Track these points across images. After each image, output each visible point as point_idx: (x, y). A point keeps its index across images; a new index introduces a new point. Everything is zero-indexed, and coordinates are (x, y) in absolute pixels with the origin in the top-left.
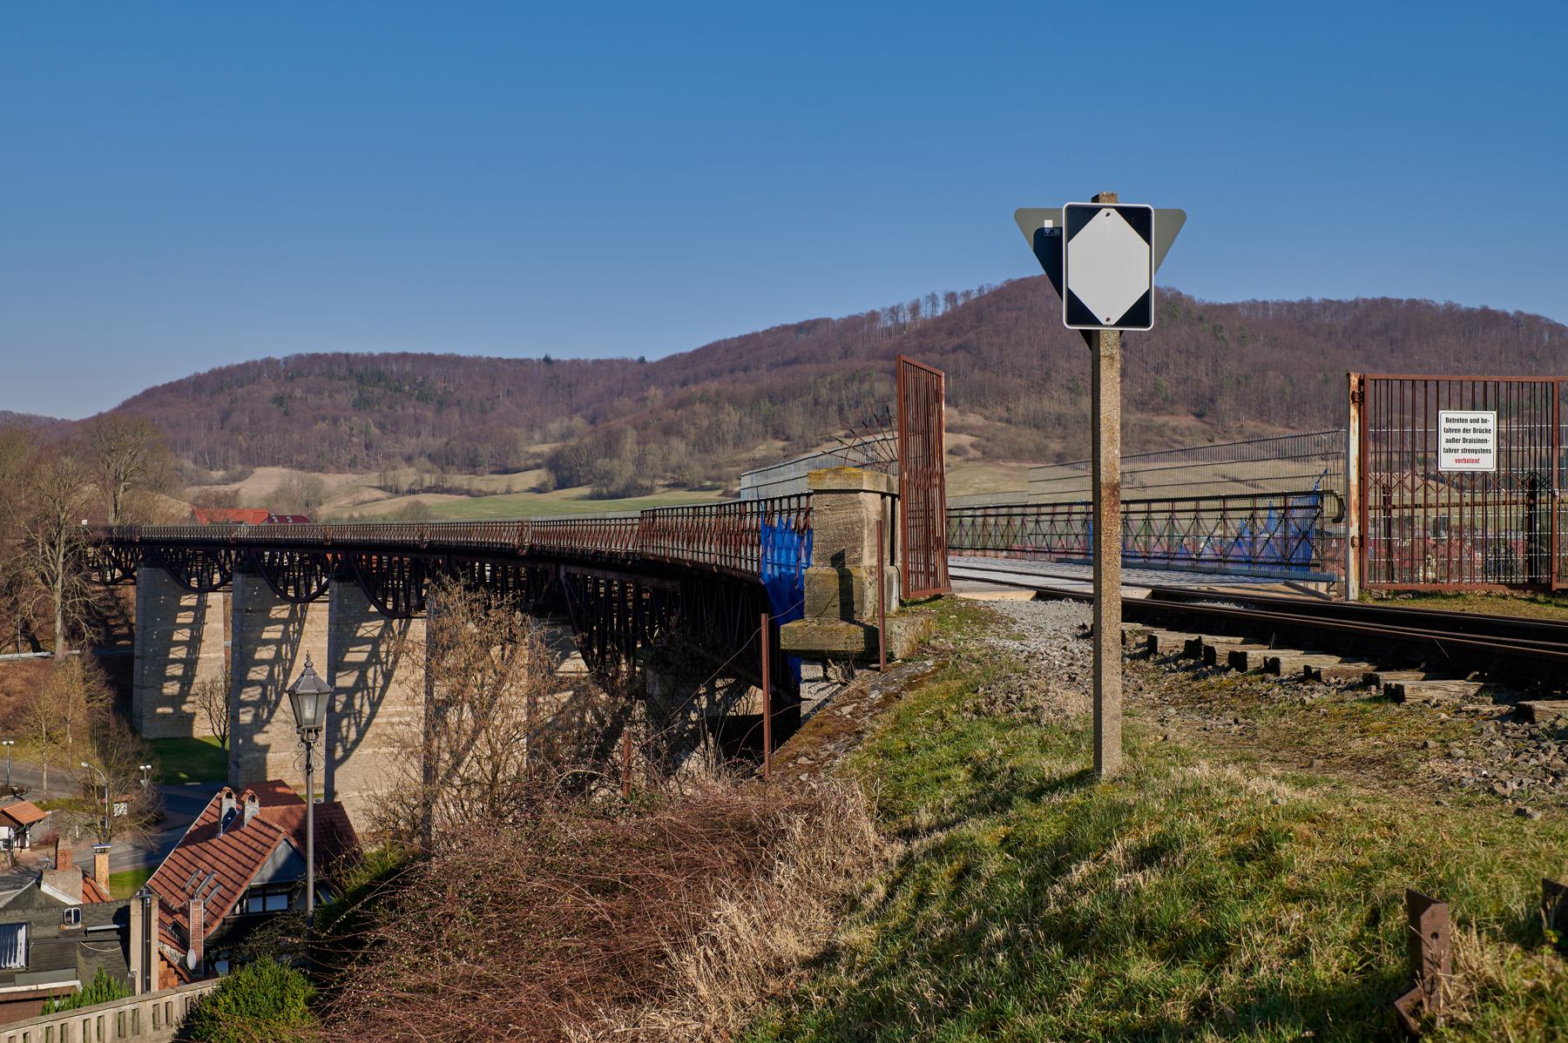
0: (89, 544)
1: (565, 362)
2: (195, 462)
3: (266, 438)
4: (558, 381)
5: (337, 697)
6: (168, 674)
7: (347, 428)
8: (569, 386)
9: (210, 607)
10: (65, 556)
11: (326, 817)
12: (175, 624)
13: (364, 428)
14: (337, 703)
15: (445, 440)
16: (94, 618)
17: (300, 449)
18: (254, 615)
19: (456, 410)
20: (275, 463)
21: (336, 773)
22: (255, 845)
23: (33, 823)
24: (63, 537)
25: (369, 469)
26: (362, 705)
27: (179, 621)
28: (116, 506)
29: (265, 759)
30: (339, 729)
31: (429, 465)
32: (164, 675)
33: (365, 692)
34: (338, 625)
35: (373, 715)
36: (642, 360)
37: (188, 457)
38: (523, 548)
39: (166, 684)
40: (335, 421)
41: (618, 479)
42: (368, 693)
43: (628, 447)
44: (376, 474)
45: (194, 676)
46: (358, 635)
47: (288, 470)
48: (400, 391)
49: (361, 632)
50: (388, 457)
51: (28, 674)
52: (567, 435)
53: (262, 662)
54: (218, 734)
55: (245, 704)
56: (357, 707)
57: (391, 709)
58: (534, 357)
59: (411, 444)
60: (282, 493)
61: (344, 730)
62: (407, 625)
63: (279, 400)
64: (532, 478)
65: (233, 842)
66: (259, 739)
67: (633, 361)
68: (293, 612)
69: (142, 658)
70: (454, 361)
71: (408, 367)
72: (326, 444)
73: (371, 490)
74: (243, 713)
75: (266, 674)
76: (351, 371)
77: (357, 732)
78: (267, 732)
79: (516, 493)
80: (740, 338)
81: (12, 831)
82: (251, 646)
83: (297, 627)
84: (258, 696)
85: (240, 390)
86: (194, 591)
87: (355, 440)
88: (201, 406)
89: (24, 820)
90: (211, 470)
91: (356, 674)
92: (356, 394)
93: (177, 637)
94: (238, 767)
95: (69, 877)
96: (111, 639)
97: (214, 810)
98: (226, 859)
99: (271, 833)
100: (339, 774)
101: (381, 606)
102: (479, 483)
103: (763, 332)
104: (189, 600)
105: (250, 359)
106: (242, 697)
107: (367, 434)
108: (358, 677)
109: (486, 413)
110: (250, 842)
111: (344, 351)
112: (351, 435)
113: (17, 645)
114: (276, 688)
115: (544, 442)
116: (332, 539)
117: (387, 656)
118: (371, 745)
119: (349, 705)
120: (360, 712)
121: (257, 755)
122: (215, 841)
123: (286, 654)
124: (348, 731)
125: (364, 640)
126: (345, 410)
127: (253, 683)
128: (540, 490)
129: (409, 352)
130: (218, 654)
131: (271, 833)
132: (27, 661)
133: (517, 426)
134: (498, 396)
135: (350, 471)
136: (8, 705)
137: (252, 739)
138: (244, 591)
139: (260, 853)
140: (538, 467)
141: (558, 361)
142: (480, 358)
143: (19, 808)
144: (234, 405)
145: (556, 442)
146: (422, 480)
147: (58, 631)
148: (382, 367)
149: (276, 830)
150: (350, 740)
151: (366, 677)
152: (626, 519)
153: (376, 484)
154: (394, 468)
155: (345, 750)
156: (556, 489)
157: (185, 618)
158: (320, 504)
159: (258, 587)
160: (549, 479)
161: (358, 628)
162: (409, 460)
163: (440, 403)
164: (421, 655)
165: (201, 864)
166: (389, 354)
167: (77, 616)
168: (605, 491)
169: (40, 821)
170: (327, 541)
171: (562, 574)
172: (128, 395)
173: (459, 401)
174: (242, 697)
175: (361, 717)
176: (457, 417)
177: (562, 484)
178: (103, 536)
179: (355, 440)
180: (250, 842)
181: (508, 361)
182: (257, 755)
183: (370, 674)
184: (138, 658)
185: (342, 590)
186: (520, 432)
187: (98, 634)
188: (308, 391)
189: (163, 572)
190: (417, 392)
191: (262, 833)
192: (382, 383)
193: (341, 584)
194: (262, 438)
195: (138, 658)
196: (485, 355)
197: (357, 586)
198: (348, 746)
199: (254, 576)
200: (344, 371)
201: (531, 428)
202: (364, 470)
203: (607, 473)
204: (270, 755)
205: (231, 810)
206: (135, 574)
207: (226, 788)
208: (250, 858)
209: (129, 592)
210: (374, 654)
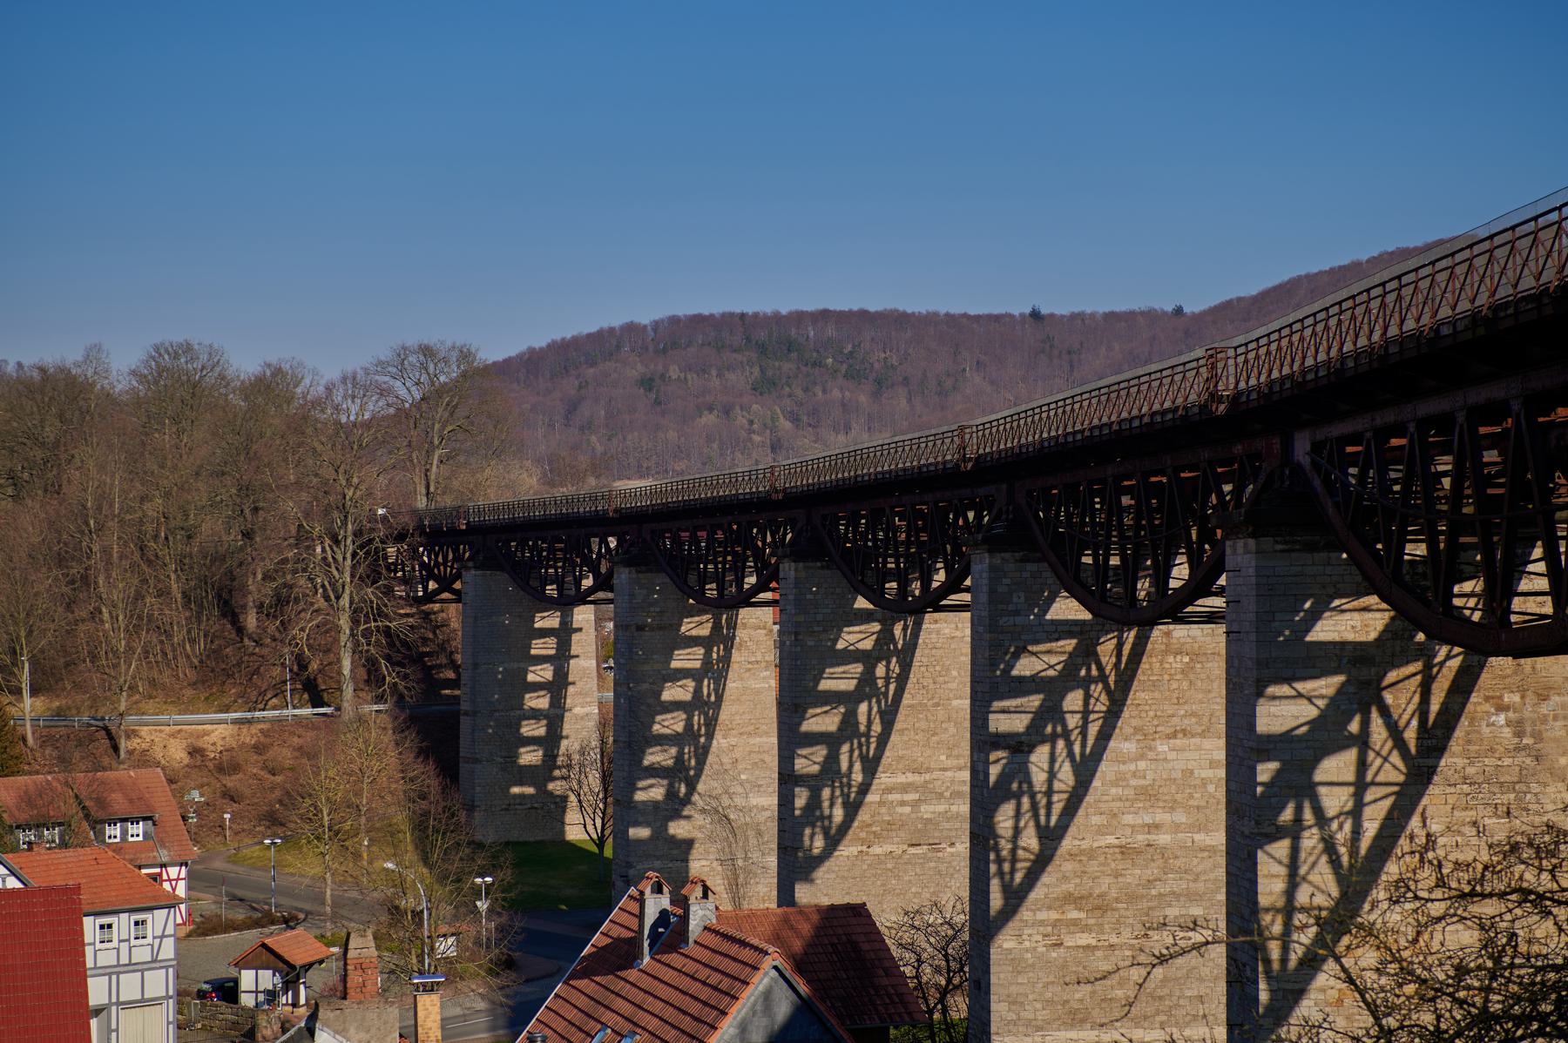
1: (1063, 316)
3: (630, 437)
7: (745, 421)
8: (1069, 353)
10: (354, 555)
11: (840, 931)
13: (769, 422)
16: (399, 651)
19: (902, 392)
22: (715, 978)
23: (311, 965)
28: (428, 487)
34: (796, 634)
36: (1179, 311)
38: (1220, 400)
40: (727, 411)
42: (860, 745)
51: (301, 741)
54: (595, 836)
58: (1016, 312)
61: (826, 804)
62: (918, 625)
63: (647, 383)
65: (669, 975)
66: (678, 829)
67: (1165, 313)
70: (897, 320)
71: (830, 331)
72: (715, 446)
75: (682, 724)
76: (748, 339)
78: (688, 817)
80: (1332, 270)
81: (278, 979)
85: (592, 370)
87: (757, 438)
88: (538, 394)
89: (298, 959)
92: (756, 370)
95: (372, 1015)
96: (431, 685)
97: (625, 919)
98: (658, 1007)
99: (746, 954)
101: (876, 596)
103: (1368, 261)
104: (548, 620)
105: (605, 325)
107: (773, 429)
110: (703, 973)
111: (738, 310)
122: (632, 974)
126: (741, 395)
130: (587, 710)
131: (746, 954)
134: (964, 370)
136: (272, 789)
138: (632, 596)
139: (727, 994)
141: (1052, 315)
142: (936, 314)
143: (288, 939)
148: (793, 331)
149: (756, 948)
159: (659, 586)
163: (879, 382)
164: (873, 733)
165: (607, 1017)
169: (321, 962)
170: (777, 491)
173: (906, 379)
176: (904, 402)
179: (757, 438)
180: (703, 973)
181: (978, 318)
184: (466, 714)
189: (502, 577)
191: (726, 955)
192: (794, 355)
193: (801, 565)
195: (466, 714)
196: (943, 311)
197: (828, 568)
205: (664, 916)
206: (457, 585)
207: (650, 874)
208: (705, 1004)
210: (867, 679)
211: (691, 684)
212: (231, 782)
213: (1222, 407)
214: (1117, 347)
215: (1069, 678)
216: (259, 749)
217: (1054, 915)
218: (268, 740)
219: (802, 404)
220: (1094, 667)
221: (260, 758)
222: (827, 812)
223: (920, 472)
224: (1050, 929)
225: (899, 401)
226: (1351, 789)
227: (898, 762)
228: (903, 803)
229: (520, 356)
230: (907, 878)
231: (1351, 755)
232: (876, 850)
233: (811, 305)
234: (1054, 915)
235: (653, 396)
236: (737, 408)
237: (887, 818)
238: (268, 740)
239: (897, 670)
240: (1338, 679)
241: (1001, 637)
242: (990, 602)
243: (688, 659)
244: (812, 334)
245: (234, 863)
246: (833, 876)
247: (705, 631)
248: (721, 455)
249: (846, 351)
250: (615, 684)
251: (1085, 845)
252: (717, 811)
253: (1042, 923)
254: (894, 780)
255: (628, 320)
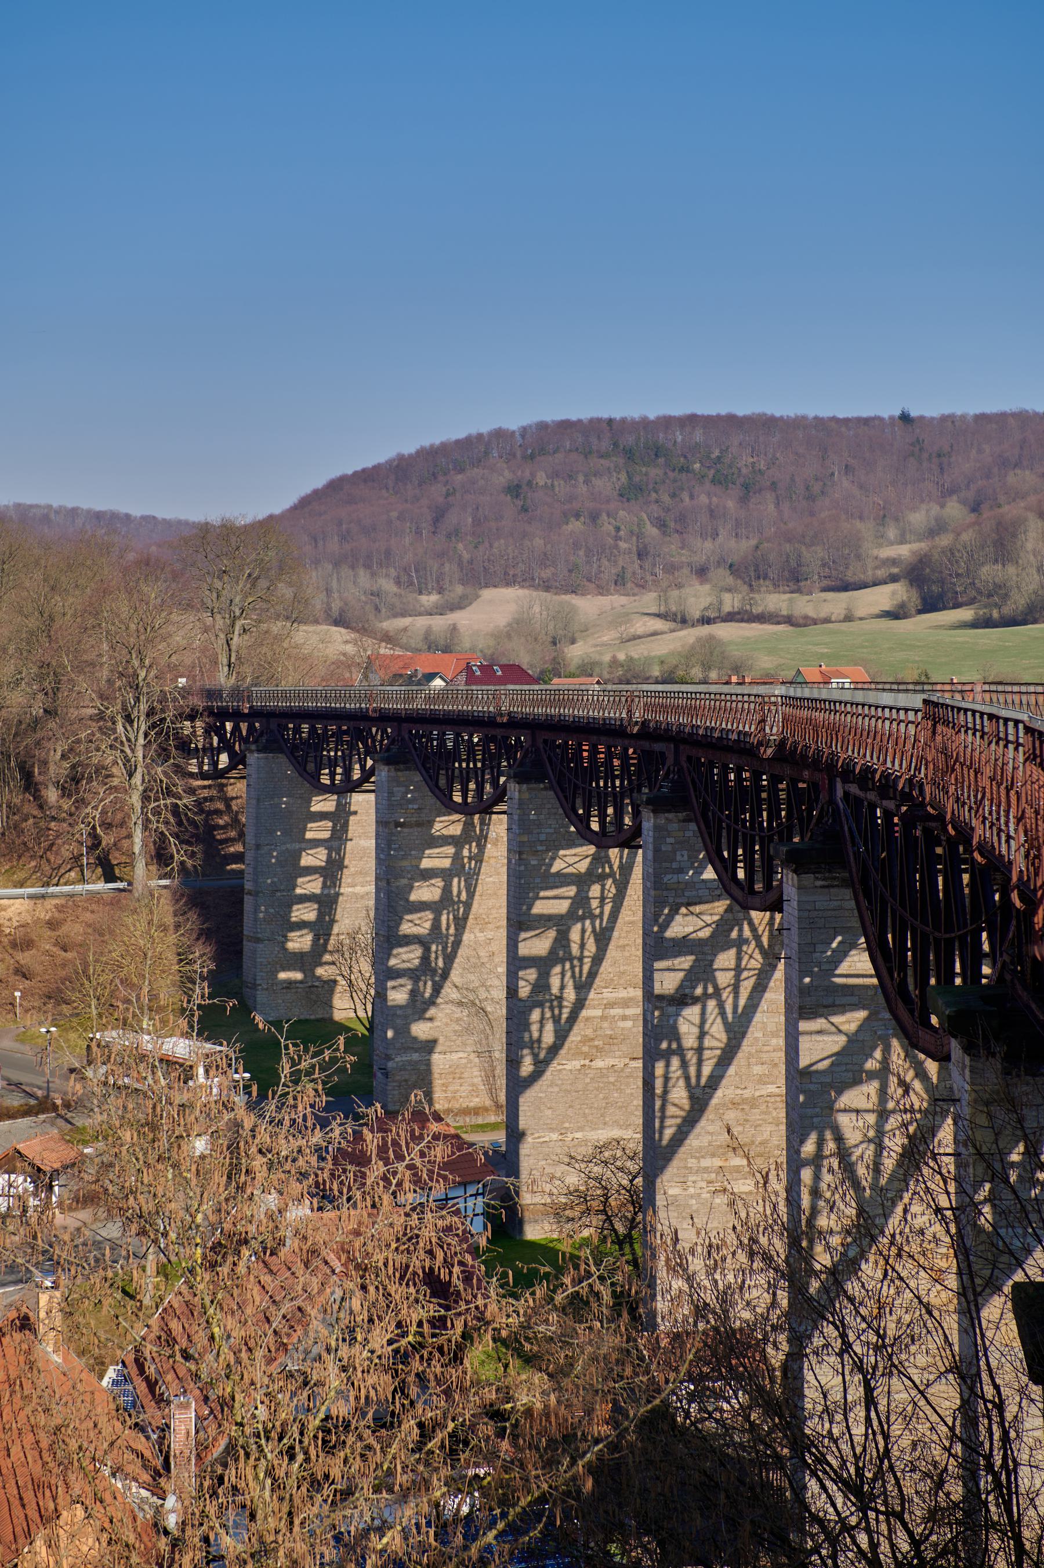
0: (181, 716)
1: (933, 419)
2: (398, 582)
3: (496, 544)
4: (922, 449)
5: (521, 973)
6: (294, 919)
7: (611, 528)
8: (939, 456)
9: (355, 813)
10: (146, 735)
12: (303, 840)
13: (635, 528)
14: (521, 983)
15: (753, 542)
17: (545, 560)
18: (406, 830)
19: (770, 497)
20: (509, 582)
21: (521, 1100)
24: (144, 707)
25: (643, 587)
26: (562, 987)
27: (309, 835)
29: (428, 1064)
30: (526, 1026)
31: (730, 580)
32: (289, 921)
33: (568, 966)
34: (520, 853)
35: (580, 1004)
37: (387, 575)
39: (291, 935)
40: (594, 517)
41: (1015, 595)
42: (572, 967)
43: (1029, 546)
44: (653, 595)
45: (333, 921)
46: (554, 870)
47: (526, 592)
48: (688, 471)
49: (557, 866)
50: (671, 569)
52: (934, 531)
53: (422, 906)
55: (396, 974)
56: (555, 990)
57: (608, 995)
58: (885, 415)
59: (705, 549)
60: (519, 626)
61: (534, 1028)
63: (514, 490)
64: (884, 597)
66: (420, 1030)
68: (468, 826)
69: (255, 894)
70: (767, 423)
71: (698, 436)
72: (581, 553)
73: (646, 618)
74: (394, 988)
75: (428, 925)
77: (556, 1031)
78: (431, 1019)
79: (861, 619)
82: (404, 881)
83: (475, 850)
84: (417, 962)
85: (460, 477)
86: (331, 789)
87: (623, 545)
90: (420, 593)
91: (552, 934)
92: (623, 477)
93: (306, 860)
94: (386, 1075)
100: (527, 1100)
102: (804, 605)
105: (474, 431)
106: (392, 962)
107: (639, 536)
108: (556, 940)
109: (814, 501)
111: (605, 415)
112: (617, 538)
113: (82, 871)
114: (445, 948)
115: (902, 541)
116: (509, 714)
117: (602, 906)
118: (578, 1054)
119: (541, 986)
120: (560, 998)
121: (415, 1056)
123: (459, 893)
124: (541, 1031)
125: (563, 879)
126: (608, 501)
127: (408, 940)
128: (895, 614)
129: (699, 412)
132: (93, 896)
133: (861, 518)
134: (833, 474)
135: (617, 592)
136: (64, 966)
137: (409, 1031)
138: (391, 793)
140: (894, 579)
141: (922, 418)
142: (804, 418)
144: (450, 498)
145: (920, 540)
146: (721, 603)
147: (137, 849)
148: (661, 435)
150: (544, 1045)
151: (568, 940)
152: (906, 710)
153: (654, 610)
154: (679, 586)
155: (537, 1062)
156: (920, 612)
157: (319, 831)
158: (573, 641)
160: (909, 598)
161: (553, 859)
162: (702, 572)
163: (746, 487)
166: (670, 417)
167: (162, 828)
168: (995, 614)
170: (501, 715)
171: (840, 793)
172: (307, 490)
173: (773, 483)
174: (392, 962)
175: (561, 1007)
176: (771, 507)
177: (930, 605)
178: (199, 703)
179: (623, 545)
181: (847, 420)
182: (415, 1056)
183: (575, 935)
184: (249, 893)
185: (526, 796)
186: (865, 528)
187: (192, 855)
188: (555, 475)
189: (282, 759)
190: (712, 471)
192: (661, 460)
194: (491, 546)
195: (249, 893)
196: (811, 414)
198: (542, 1055)
199: (408, 769)
200: (605, 445)
201: (882, 520)
202: (636, 590)
203: (998, 586)
204: (436, 1058)
209: (237, 789)
210: (581, 901)
211: (439, 882)
212: (24, 958)
213: (769, 751)
214: (988, 451)
215: (720, 939)
216: (52, 924)
217: (717, 1162)
218: (62, 916)
219: (669, 510)
220: (746, 927)
221: (53, 934)
222: (536, 1035)
223: (605, 724)
224: (713, 1175)
225: (767, 506)
226: (732, 973)
227: (620, 978)
228: (624, 1018)
229: (389, 462)
230: (628, 1091)
231: (732, 952)
232: (599, 1063)
233: (678, 410)
234: (717, 1162)
235: (520, 503)
236: (604, 515)
237: (609, 1032)
238: (62, 916)
239: (613, 890)
240: (862, 1014)
241: (665, 893)
242: (655, 861)
243: (436, 859)
244: (679, 439)
245: (22, 1042)
246: (556, 1089)
247: (456, 830)
248: (588, 562)
249: (713, 456)
250: (377, 878)
251: (747, 1094)
252: (474, 1004)
253: (706, 1170)
254: (613, 995)
255: (496, 426)
